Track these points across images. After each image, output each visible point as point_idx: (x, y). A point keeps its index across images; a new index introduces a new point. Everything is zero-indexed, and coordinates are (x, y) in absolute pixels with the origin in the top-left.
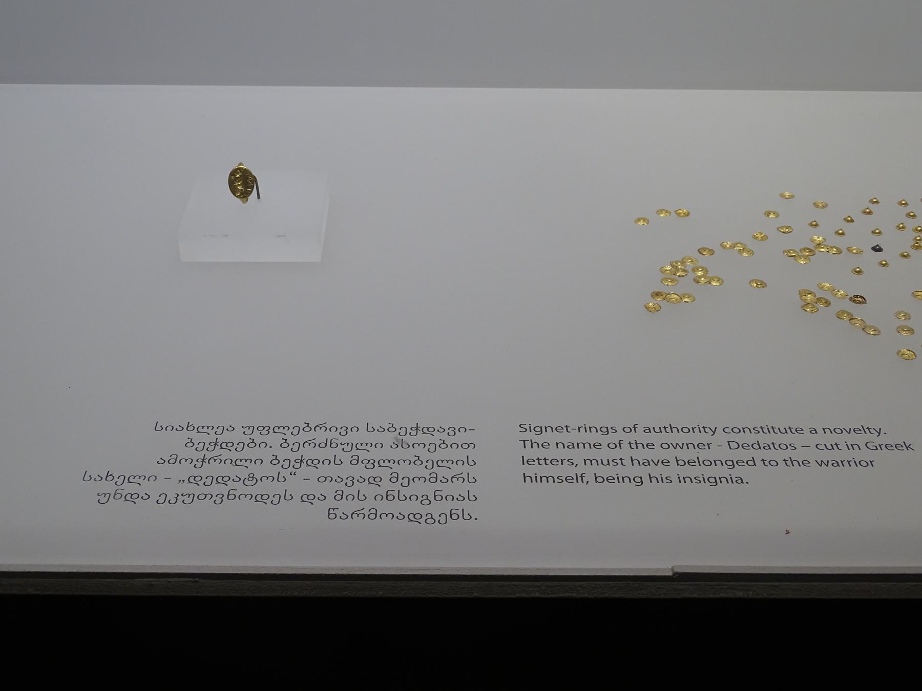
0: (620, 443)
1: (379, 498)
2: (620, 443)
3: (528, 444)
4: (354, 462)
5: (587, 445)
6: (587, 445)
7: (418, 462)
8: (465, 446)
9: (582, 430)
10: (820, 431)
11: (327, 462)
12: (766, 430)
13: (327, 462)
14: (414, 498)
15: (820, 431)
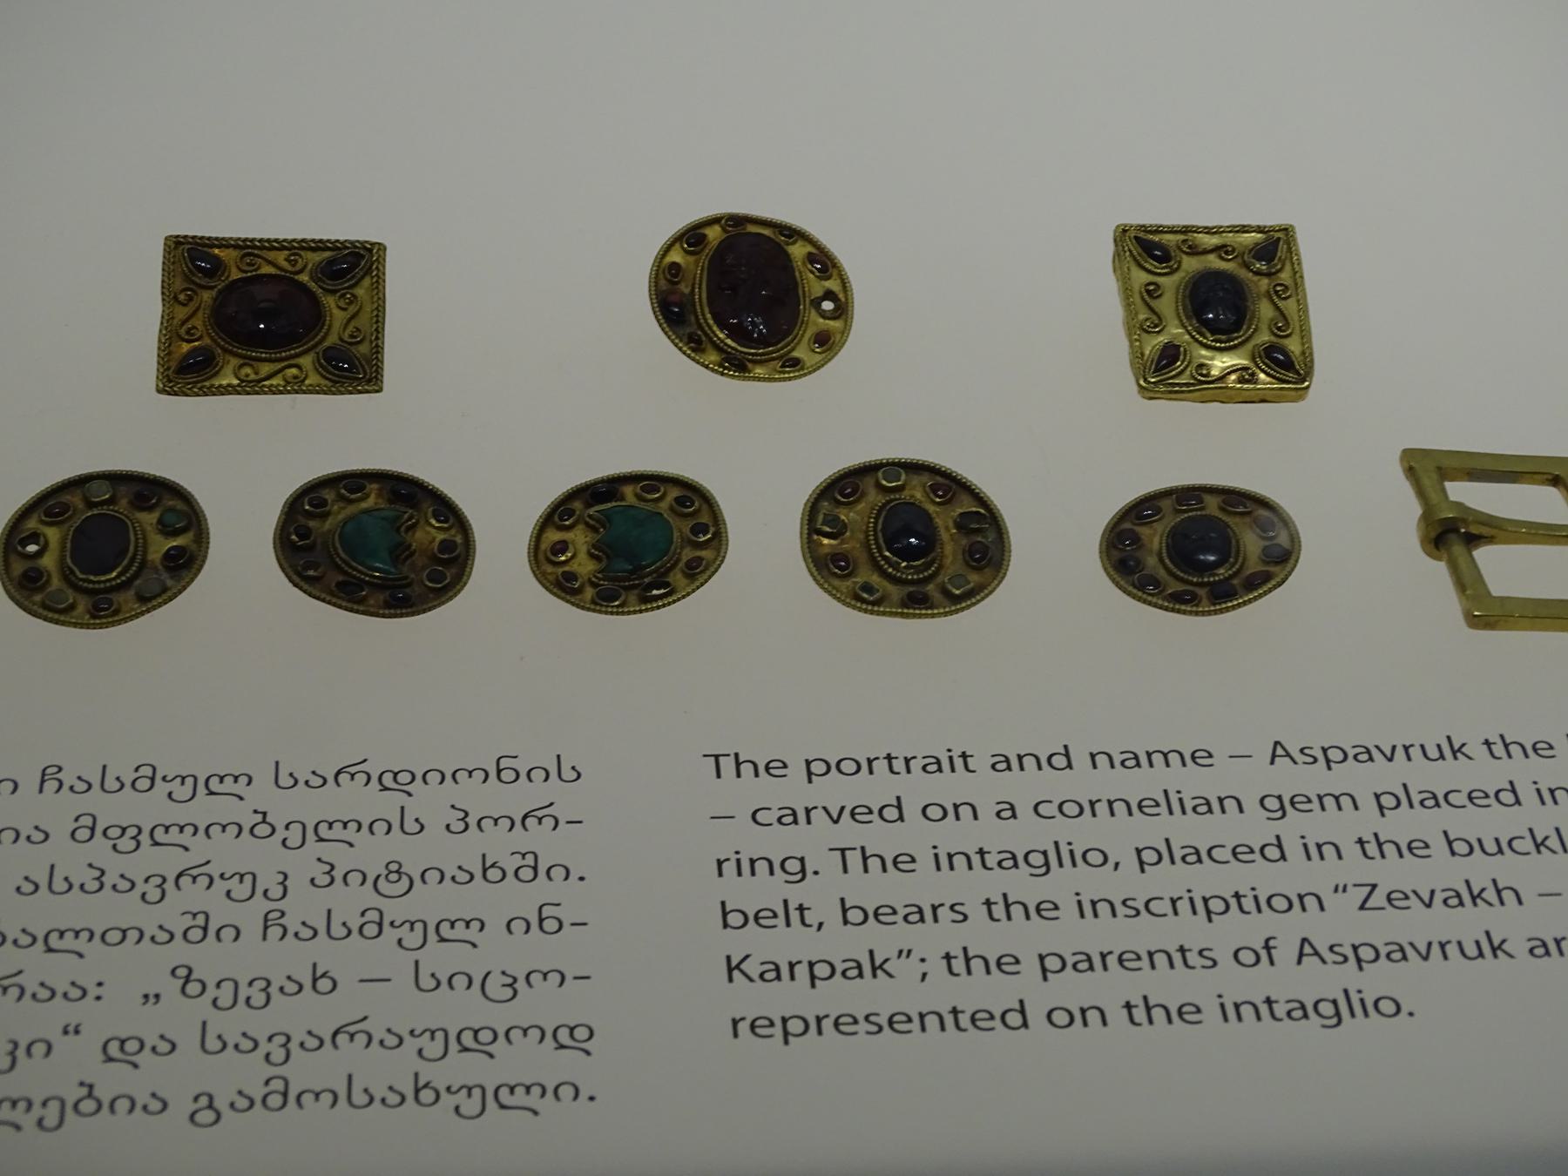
0: (1267, 947)
1: (518, 926)
2: (1267, 947)
3: (854, 859)
4: (83, 834)
5: (1174, 758)
6: (1174, 758)
7: (263, 830)
8: (114, 936)
9: (730, 868)
10: (1476, 749)
11: (380, 827)
12: (1248, 904)
13: (380, 827)
14: (460, 982)
15: (1476, 749)
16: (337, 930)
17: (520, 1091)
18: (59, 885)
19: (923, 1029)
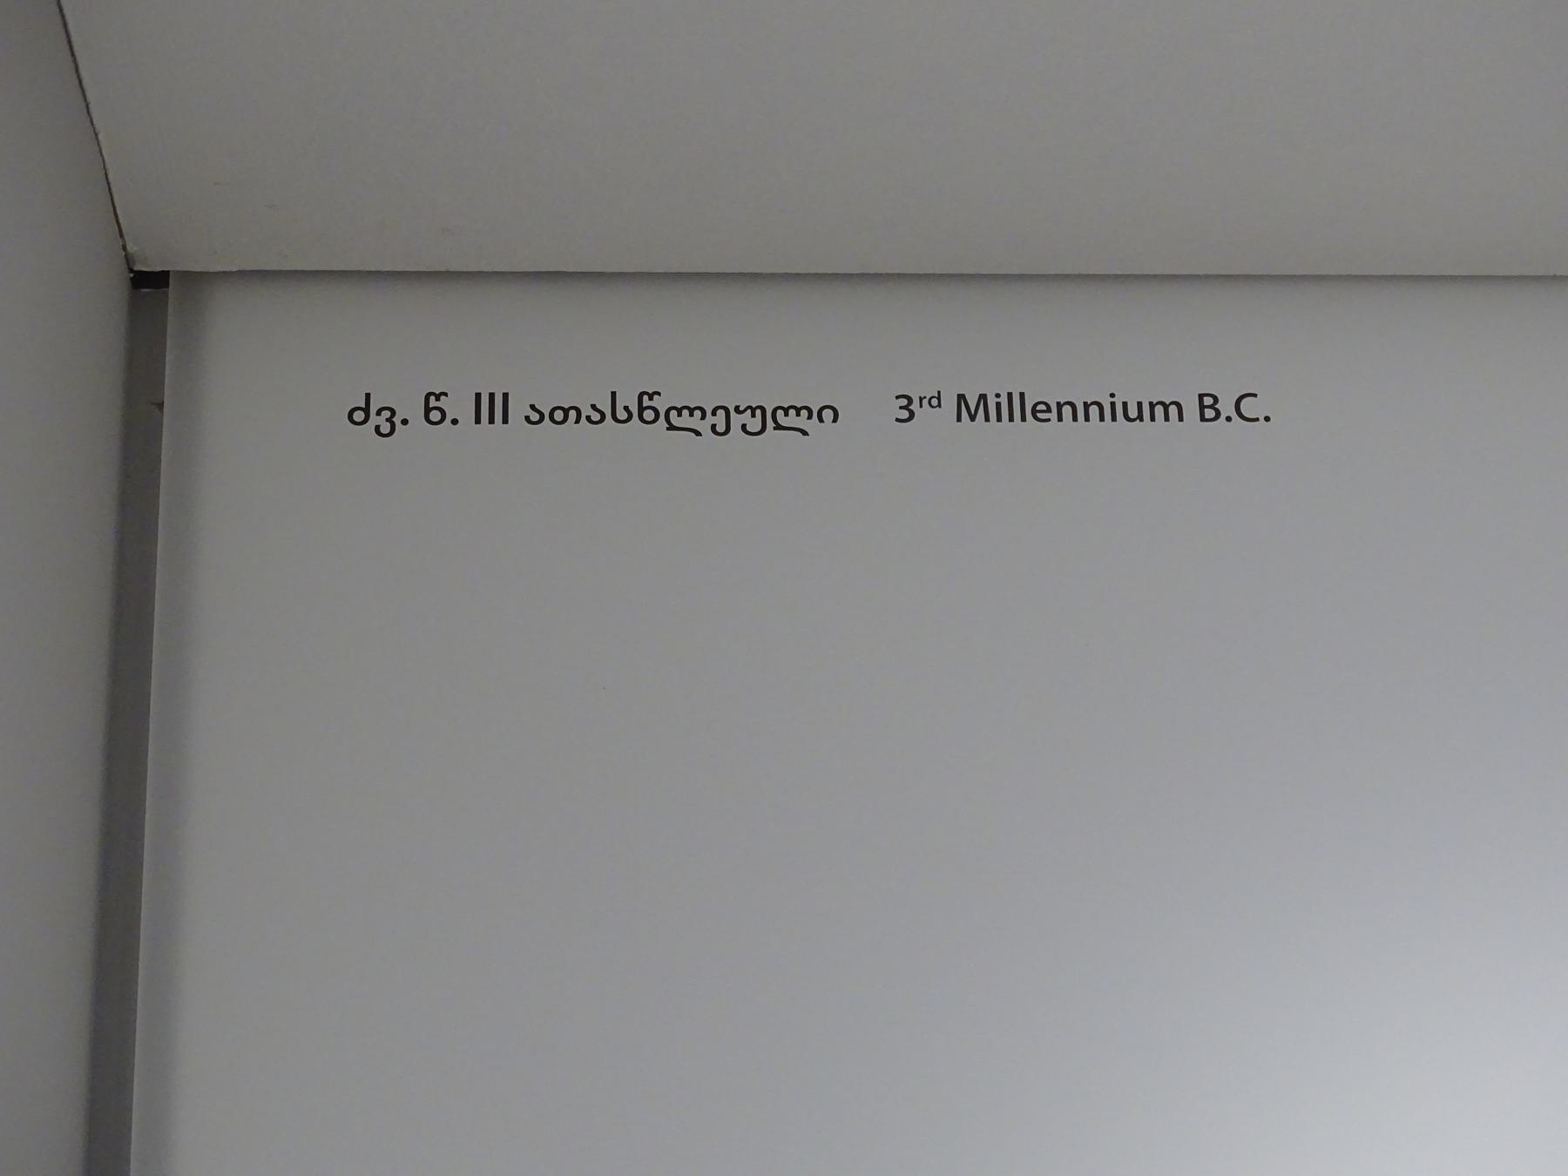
8: (559, 415)
16: (622, 415)
17: (792, 412)
18: (622, 415)
19: (1060, 419)
